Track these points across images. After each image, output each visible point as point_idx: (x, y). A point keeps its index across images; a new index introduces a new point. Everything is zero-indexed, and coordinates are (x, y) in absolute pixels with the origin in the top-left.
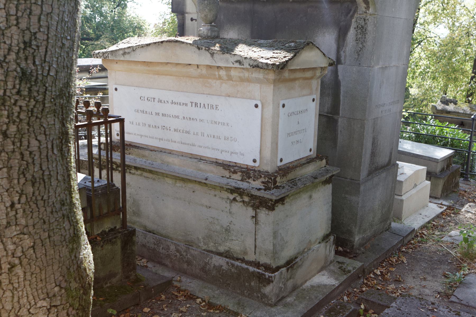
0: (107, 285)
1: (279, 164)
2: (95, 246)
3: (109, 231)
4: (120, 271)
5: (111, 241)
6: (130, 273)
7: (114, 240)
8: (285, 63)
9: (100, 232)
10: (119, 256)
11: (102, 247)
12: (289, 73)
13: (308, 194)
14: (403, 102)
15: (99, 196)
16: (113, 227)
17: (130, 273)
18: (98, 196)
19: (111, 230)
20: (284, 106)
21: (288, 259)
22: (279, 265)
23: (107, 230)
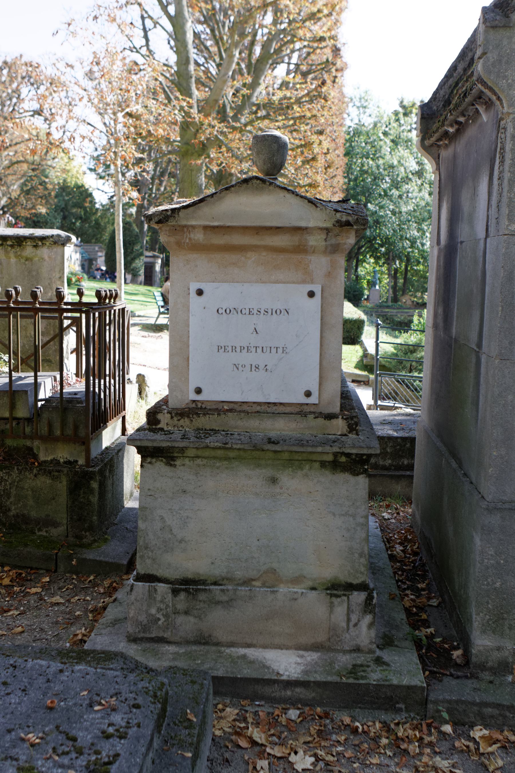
0: (40, 533)
1: (193, 396)
2: (25, 472)
3: (65, 463)
4: (65, 522)
5: (50, 473)
6: (83, 533)
7: (56, 474)
8: (169, 213)
9: (49, 459)
10: (63, 498)
11: (35, 476)
12: (204, 234)
13: (269, 472)
14: (370, 297)
15: (50, 409)
16: (72, 459)
17: (83, 533)
18: (49, 408)
19: (68, 462)
20: (200, 292)
21: (190, 577)
22: (155, 573)
23: (62, 460)
